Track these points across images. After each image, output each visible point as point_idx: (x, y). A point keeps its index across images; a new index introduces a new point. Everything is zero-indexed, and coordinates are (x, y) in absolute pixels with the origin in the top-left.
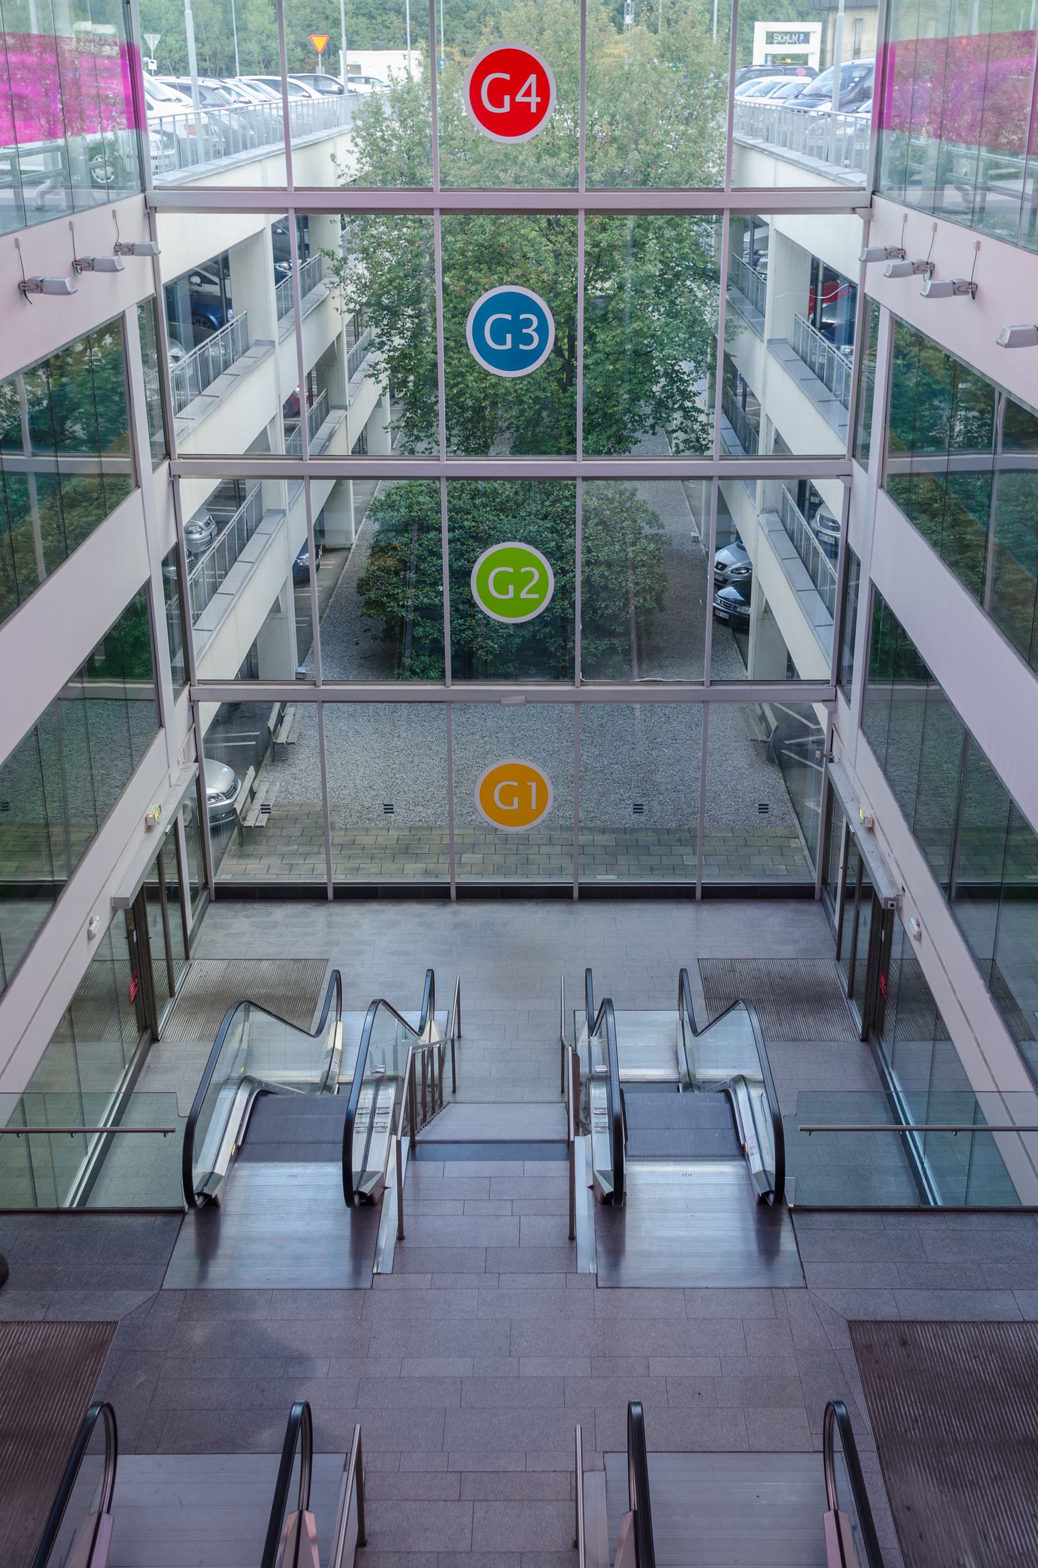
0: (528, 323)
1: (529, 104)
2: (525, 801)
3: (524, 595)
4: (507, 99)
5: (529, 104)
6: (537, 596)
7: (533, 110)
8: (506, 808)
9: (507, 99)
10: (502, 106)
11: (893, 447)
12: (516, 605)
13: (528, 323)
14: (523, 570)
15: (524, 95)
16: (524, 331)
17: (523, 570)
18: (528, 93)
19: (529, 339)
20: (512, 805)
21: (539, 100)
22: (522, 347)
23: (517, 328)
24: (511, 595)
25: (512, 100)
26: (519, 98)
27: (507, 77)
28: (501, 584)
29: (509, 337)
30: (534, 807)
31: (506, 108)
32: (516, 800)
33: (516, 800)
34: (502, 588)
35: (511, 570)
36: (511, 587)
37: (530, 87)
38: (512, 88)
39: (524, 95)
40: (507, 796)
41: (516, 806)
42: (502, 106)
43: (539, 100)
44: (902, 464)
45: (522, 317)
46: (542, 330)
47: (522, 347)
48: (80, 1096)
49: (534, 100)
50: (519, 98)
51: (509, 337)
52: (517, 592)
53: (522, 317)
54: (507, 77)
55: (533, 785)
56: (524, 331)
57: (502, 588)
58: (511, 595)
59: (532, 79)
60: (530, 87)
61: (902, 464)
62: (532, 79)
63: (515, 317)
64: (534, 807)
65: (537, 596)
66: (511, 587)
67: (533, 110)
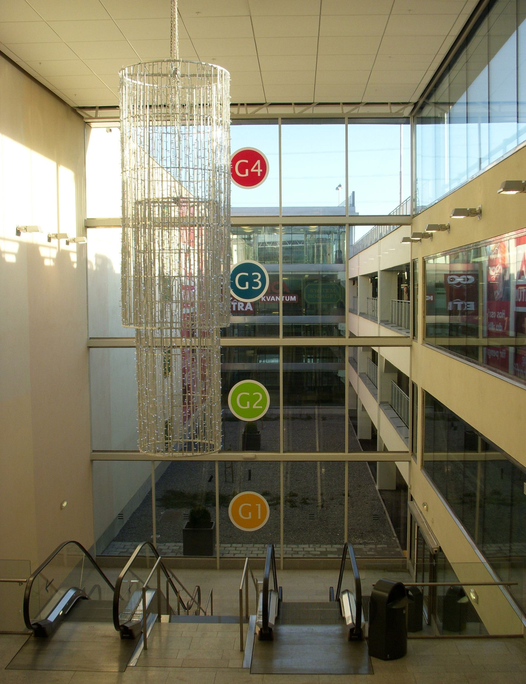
0: (256, 277)
1: (257, 173)
2: (255, 514)
3: (254, 407)
4: (247, 171)
5: (257, 173)
6: (261, 407)
7: (259, 175)
8: (244, 408)
9: (247, 171)
10: (245, 173)
11: (426, 449)
12: (252, 412)
13: (256, 277)
14: (254, 394)
15: (255, 169)
16: (254, 280)
17: (254, 394)
18: (256, 168)
19: (257, 284)
20: (245, 286)
21: (261, 170)
22: (253, 288)
23: (250, 279)
24: (248, 407)
25: (249, 171)
26: (253, 170)
27: (247, 161)
28: (243, 401)
29: (247, 283)
30: (259, 518)
31: (247, 174)
32: (250, 513)
33: (250, 513)
34: (244, 404)
35: (247, 274)
36: (248, 403)
37: (257, 165)
38: (249, 166)
39: (255, 169)
40: (242, 282)
41: (250, 517)
42: (245, 173)
43: (261, 170)
44: (430, 456)
45: (253, 274)
46: (263, 280)
47: (253, 288)
48: (50, 583)
49: (259, 171)
50: (253, 170)
51: (247, 283)
52: (251, 406)
53: (253, 274)
54: (247, 161)
55: (259, 505)
56: (254, 280)
57: (244, 404)
58: (248, 407)
59: (258, 162)
60: (257, 165)
61: (430, 456)
62: (258, 162)
63: (250, 274)
64: (259, 518)
65: (261, 407)
66: (248, 403)
67: (259, 175)
